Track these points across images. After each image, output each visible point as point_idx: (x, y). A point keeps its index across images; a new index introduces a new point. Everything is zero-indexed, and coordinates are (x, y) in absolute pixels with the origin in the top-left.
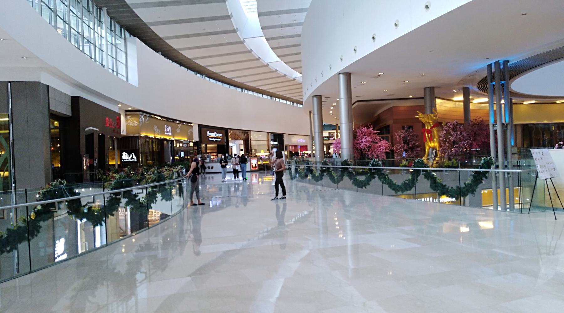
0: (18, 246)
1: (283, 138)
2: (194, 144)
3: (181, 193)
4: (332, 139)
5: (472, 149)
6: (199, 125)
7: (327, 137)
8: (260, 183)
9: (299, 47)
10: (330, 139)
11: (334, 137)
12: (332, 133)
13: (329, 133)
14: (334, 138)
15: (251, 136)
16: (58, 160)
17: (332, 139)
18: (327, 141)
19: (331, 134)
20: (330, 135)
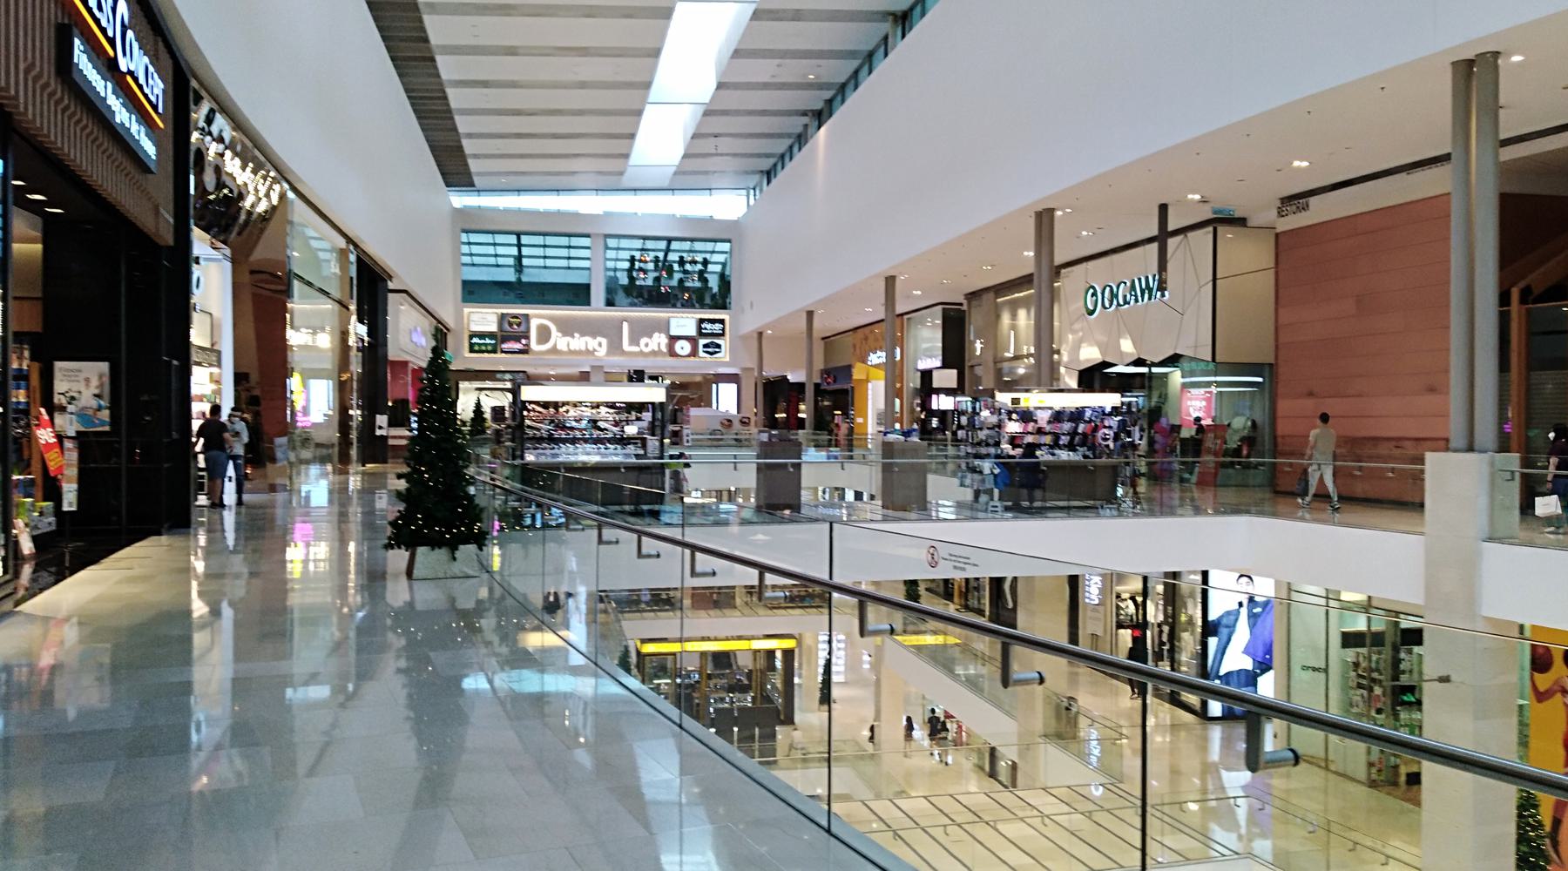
0: (1396, 797)
1: (386, 315)
2: (1119, 346)
3: (964, 590)
4: (517, 346)
5: (389, 371)
6: (856, 492)
7: (491, 335)
8: (820, 489)
9: (818, 695)
10: (505, 346)
11: (527, 338)
12: (515, 317)
13: (503, 317)
14: (527, 345)
15: (970, 324)
16: (934, 325)
17: (517, 346)
18: (486, 355)
19: (511, 324)
20: (507, 327)
